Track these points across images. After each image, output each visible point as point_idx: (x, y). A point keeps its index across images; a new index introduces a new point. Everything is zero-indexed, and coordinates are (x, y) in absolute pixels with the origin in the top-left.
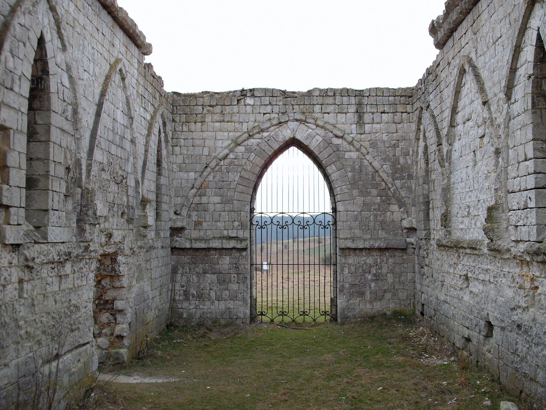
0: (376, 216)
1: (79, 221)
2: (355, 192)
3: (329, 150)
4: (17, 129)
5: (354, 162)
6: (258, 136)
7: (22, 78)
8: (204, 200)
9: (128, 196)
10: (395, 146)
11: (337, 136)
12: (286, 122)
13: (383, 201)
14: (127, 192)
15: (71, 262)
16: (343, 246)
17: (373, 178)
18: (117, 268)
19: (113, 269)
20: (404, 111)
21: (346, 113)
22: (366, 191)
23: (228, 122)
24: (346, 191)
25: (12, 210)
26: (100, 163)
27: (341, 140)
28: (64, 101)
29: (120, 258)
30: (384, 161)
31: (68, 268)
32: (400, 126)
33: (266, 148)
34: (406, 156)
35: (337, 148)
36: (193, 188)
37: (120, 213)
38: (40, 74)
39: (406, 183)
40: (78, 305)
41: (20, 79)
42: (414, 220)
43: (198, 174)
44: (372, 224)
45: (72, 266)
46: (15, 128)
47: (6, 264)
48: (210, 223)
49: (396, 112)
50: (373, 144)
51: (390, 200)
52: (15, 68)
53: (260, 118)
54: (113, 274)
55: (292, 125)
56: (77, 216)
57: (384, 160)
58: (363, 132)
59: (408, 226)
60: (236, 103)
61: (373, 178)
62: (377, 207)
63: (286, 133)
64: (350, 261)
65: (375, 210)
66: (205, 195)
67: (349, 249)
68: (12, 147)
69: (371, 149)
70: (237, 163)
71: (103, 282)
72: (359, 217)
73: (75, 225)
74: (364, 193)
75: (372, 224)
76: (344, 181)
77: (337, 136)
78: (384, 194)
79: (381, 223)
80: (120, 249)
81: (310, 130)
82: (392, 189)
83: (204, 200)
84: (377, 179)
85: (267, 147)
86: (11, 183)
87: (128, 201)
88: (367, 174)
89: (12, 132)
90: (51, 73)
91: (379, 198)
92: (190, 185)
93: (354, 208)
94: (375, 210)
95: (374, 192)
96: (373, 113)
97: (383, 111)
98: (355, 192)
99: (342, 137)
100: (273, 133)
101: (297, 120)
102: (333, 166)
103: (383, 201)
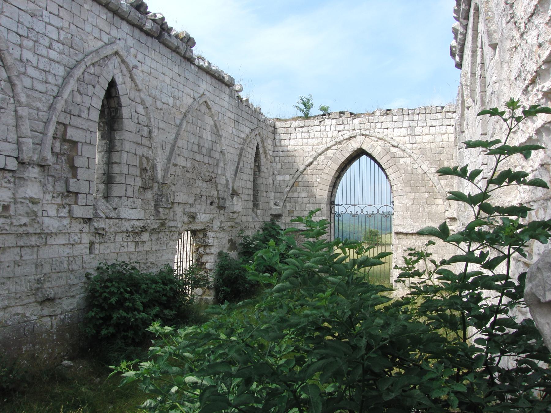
0: (424, 208)
1: (156, 206)
2: (408, 189)
3: (388, 157)
4: (86, 142)
5: (407, 166)
6: (334, 148)
7: (91, 109)
8: (295, 195)
9: (218, 191)
10: (441, 153)
11: (393, 146)
12: (354, 137)
13: (430, 197)
14: (217, 188)
15: (148, 234)
16: (397, 231)
17: (423, 178)
18: (207, 240)
19: (204, 241)
20: (449, 124)
21: (401, 128)
22: (417, 189)
23: (313, 138)
24: (401, 188)
25: (80, 196)
26: (183, 167)
27: (397, 149)
28: (139, 124)
29: (210, 234)
30: (431, 165)
31: (145, 236)
32: (444, 136)
33: (340, 157)
34: (450, 160)
35: (394, 156)
36: (287, 186)
37: (209, 202)
38: (117, 106)
39: (449, 181)
40: (154, 262)
41: (89, 109)
42: (455, 212)
43: (291, 177)
44: (420, 214)
45: (150, 236)
46: (84, 141)
47: (77, 231)
48: (299, 212)
49: (442, 125)
50: (423, 151)
51: (436, 195)
52: (83, 102)
53: (335, 134)
54: (204, 244)
55: (360, 139)
56: (155, 202)
57: (432, 164)
58: (414, 142)
59: (450, 217)
60: (318, 124)
61: (423, 178)
62: (425, 200)
63: (354, 145)
64: (403, 243)
65: (423, 203)
66: (296, 192)
67: (402, 233)
68: (80, 154)
69: (421, 155)
70: (318, 168)
71: (200, 250)
72: (411, 209)
73: (153, 208)
74: (415, 189)
75: (420, 214)
76: (399, 181)
77: (393, 146)
78: (431, 191)
79: (428, 213)
80: (208, 226)
81: (373, 142)
82: (437, 187)
83: (295, 195)
84: (426, 179)
85: (341, 156)
86: (79, 177)
87: (218, 194)
88: (417, 175)
89: (80, 144)
90: (123, 105)
91: (427, 194)
92: (286, 185)
93: (407, 201)
94: (423, 203)
95: (424, 189)
96: (423, 127)
97: (431, 125)
98: (408, 189)
99: (397, 147)
100: (345, 145)
101: (363, 135)
102: (390, 169)
103: (430, 197)
